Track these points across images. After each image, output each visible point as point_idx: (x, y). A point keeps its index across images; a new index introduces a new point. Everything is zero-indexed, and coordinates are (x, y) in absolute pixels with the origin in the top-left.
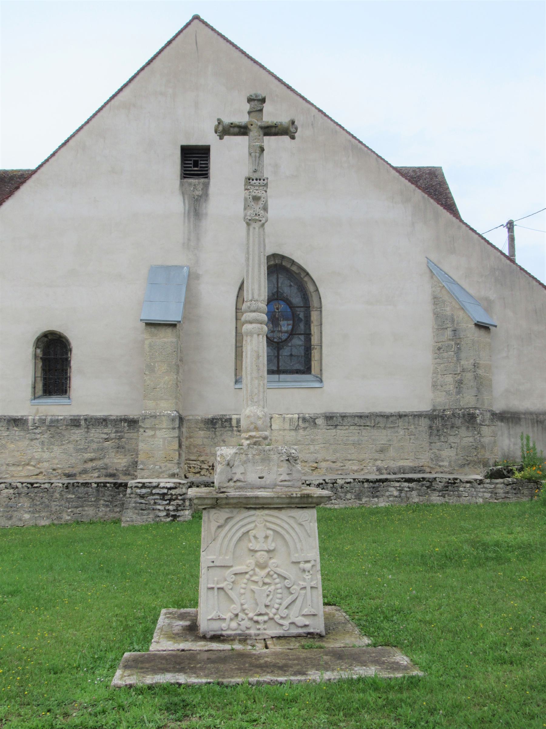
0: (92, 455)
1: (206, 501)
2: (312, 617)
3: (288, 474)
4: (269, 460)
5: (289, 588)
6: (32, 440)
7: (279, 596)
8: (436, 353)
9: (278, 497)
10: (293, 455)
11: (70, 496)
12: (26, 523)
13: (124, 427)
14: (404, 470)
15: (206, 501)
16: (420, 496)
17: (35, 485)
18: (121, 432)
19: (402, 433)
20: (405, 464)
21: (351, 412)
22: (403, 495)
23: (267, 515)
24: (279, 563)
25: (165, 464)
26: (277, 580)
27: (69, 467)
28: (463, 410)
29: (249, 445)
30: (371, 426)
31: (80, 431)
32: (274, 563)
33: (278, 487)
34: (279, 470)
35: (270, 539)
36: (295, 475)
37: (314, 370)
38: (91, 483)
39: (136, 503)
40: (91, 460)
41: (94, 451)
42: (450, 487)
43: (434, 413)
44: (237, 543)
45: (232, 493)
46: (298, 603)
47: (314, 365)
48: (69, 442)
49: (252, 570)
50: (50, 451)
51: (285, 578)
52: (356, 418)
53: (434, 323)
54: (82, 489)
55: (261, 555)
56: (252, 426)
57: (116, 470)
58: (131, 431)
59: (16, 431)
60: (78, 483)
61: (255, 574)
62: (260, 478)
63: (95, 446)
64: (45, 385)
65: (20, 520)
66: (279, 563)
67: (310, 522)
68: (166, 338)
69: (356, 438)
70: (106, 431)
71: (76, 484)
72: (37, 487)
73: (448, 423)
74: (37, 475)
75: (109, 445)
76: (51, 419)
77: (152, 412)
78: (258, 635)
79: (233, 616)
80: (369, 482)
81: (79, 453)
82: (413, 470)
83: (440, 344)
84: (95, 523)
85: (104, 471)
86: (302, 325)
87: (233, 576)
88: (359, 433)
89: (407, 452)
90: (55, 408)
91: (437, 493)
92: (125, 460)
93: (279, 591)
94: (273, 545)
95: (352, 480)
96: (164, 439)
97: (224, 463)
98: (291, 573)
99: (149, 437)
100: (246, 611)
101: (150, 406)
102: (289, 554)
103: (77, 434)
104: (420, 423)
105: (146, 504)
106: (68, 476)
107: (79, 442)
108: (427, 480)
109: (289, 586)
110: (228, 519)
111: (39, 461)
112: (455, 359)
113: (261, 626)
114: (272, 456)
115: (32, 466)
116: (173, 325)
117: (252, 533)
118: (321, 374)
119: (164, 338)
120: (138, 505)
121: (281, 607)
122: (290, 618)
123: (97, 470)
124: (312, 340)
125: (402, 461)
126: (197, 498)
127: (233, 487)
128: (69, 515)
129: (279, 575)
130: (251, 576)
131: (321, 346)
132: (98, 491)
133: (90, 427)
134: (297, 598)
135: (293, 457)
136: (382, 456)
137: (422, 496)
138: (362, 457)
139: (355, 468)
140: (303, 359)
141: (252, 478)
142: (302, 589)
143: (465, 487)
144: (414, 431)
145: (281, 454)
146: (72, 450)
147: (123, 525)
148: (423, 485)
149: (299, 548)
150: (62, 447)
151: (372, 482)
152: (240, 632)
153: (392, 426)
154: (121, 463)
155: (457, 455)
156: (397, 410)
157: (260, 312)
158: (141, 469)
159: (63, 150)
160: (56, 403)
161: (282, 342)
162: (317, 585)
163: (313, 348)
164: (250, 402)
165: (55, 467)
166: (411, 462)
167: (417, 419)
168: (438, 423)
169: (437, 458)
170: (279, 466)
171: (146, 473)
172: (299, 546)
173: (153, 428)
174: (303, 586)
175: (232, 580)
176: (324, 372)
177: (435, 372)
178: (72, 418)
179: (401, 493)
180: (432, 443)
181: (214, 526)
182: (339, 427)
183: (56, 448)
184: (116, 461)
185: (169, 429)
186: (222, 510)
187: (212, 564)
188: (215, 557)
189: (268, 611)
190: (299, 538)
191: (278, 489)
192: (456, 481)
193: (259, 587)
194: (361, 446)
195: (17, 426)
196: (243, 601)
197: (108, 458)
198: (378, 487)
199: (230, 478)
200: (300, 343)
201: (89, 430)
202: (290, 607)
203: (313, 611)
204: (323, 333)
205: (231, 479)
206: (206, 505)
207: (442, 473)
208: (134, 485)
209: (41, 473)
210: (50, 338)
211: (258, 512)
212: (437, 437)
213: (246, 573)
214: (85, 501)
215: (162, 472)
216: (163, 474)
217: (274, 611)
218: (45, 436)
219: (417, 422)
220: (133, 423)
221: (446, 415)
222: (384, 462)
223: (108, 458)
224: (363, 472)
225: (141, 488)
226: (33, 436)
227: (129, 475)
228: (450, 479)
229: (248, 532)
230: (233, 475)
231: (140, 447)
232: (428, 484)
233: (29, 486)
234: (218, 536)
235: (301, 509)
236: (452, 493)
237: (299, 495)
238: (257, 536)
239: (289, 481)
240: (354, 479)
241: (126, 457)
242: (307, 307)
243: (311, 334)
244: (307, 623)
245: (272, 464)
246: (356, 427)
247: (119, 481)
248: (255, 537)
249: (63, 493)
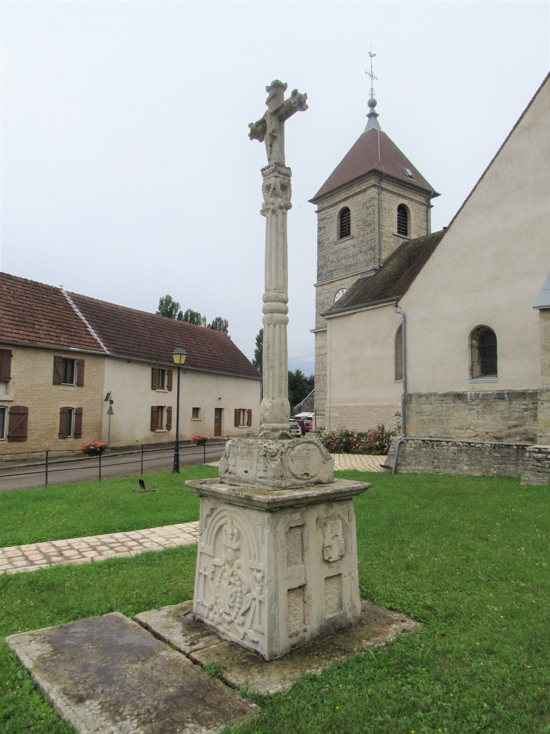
0: (514, 422)
6: (470, 410)
11: (496, 455)
12: (465, 473)
17: (472, 445)
38: (512, 445)
39: (533, 465)
40: (515, 426)
41: (516, 419)
48: (497, 412)
54: (505, 450)
59: (460, 404)
60: (502, 445)
63: (516, 415)
64: (482, 368)
65: (461, 470)
70: (524, 402)
71: (501, 446)
74: (475, 437)
76: (483, 394)
85: (524, 436)
90: (488, 385)
94: (237, 544)
99: (546, 408)
103: (502, 405)
105: (542, 467)
106: (497, 438)
111: (476, 426)
115: (471, 429)
120: (535, 467)
128: (495, 470)
132: (518, 452)
133: (512, 399)
147: (522, 483)
150: (492, 415)
157: (271, 301)
158: (540, 436)
159: (481, 183)
165: (487, 431)
171: (544, 440)
178: (498, 392)
183: (487, 416)
195: (460, 399)
208: (532, 450)
209: (478, 435)
214: (507, 459)
225: (538, 453)
226: (471, 407)
233: (467, 445)
239: (265, 478)
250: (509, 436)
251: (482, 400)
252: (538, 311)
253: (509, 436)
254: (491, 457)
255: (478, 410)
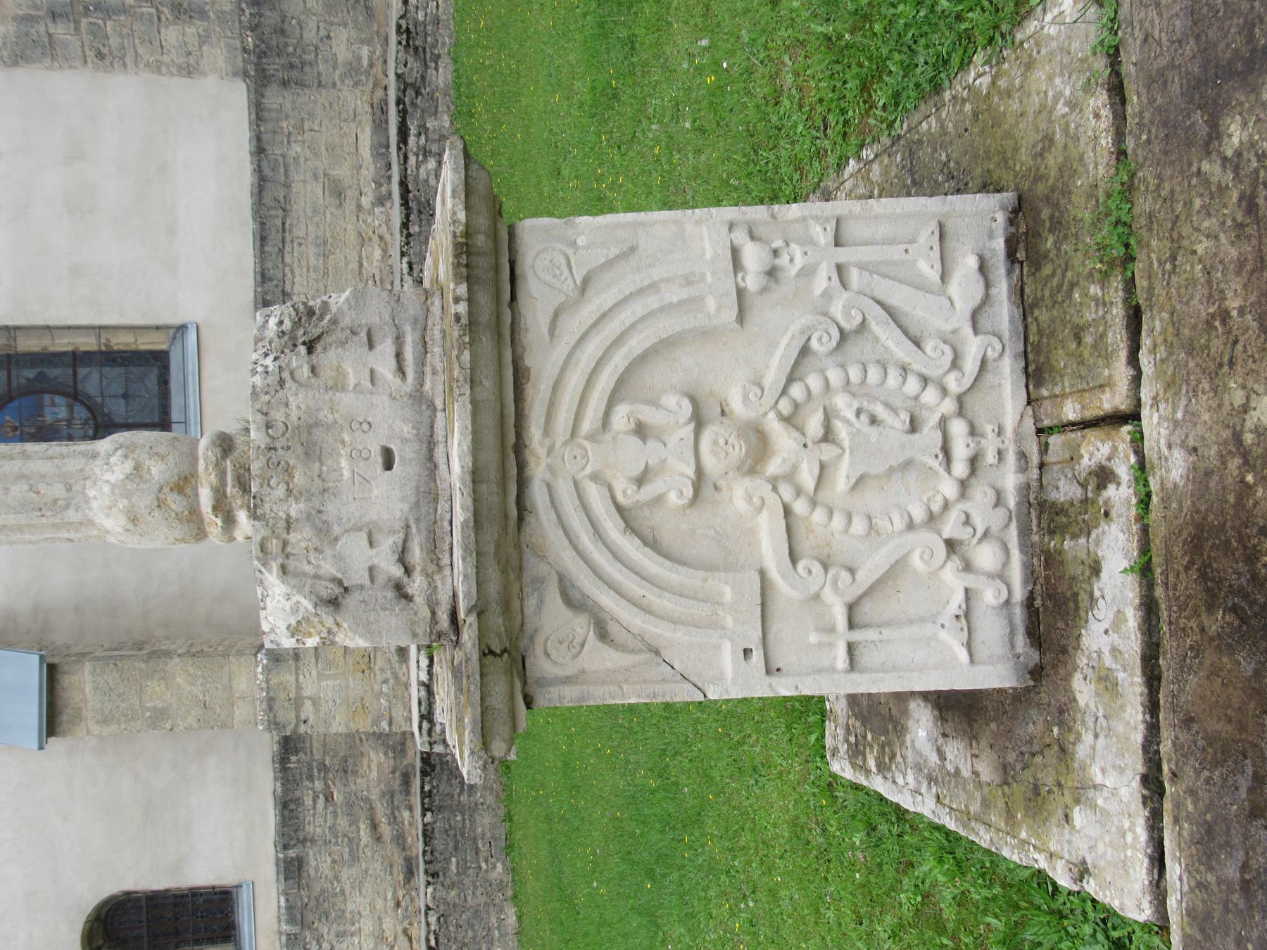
0: (362, 826)
1: (498, 700)
2: (951, 243)
3: (371, 345)
4: (310, 427)
5: (843, 335)
7: (874, 375)
8: (112, 64)
9: (473, 383)
10: (288, 325)
11: (453, 868)
13: (299, 761)
14: (381, 145)
15: (498, 700)
16: (436, 112)
17: (433, 943)
18: (310, 769)
19: (297, 148)
20: (368, 143)
21: (252, 259)
22: (434, 148)
23: (547, 432)
24: (743, 377)
25: (378, 672)
26: (814, 382)
27: (391, 873)
28: (244, 6)
29: (254, 516)
30: (284, 218)
31: (311, 856)
32: (745, 398)
33: (427, 386)
34: (352, 381)
35: (648, 415)
36: (376, 312)
37: (159, 343)
38: (425, 825)
40: (374, 826)
41: (354, 822)
42: (417, 43)
43: (252, 73)
44: (666, 556)
45: (458, 579)
46: (897, 296)
47: (146, 343)
48: (336, 878)
49: (775, 489)
50: (357, 917)
51: (805, 351)
52: (267, 249)
53: (38, 65)
54: (438, 843)
55: (715, 454)
56: (176, 502)
57: (393, 772)
58: (308, 745)
60: (424, 852)
61: (790, 476)
62: (388, 465)
63: (343, 823)
66: (743, 377)
67: (573, 244)
68: (84, 685)
69: (312, 251)
70: (308, 802)
71: (428, 857)
72: (436, 939)
73: (274, 43)
74: (410, 940)
75: (339, 791)
76: (288, 922)
77: (260, 707)
78: (1022, 456)
79: (956, 562)
80: (408, 221)
81: (361, 854)
82: (380, 125)
83: (88, 53)
84: (509, 813)
85: (398, 798)
86: (54, 373)
87: (801, 565)
88: (300, 244)
89: (341, 138)
91: (431, 72)
92: (372, 755)
93: (855, 374)
94: (671, 400)
95: (405, 260)
96: (320, 676)
97: (329, 622)
98: (781, 328)
99: (317, 711)
100: (936, 507)
101: (247, 712)
102: (707, 334)
103: (319, 863)
104: (275, 106)
106: (410, 873)
107: (336, 857)
108: (401, 95)
109: (836, 334)
110: (574, 601)
112: (122, 18)
113: (990, 447)
114: (294, 414)
116: (52, 673)
117: (626, 493)
118: (167, 327)
119: (83, 691)
121: (916, 367)
122: (954, 332)
123: (397, 813)
124: (88, 348)
125: (361, 150)
126: (486, 746)
127: (429, 576)
128: (495, 867)
129: (791, 379)
130: (799, 492)
131: (100, 328)
132: (440, 808)
133: (301, 835)
134: (878, 302)
135: (297, 324)
136: (350, 193)
137: (437, 107)
138: (352, 238)
139: (378, 253)
140: (134, 369)
141: (387, 499)
142: (844, 285)
143: (417, 8)
144: (293, 122)
145: (286, 375)
146: (354, 871)
148: (413, 104)
149: (683, 294)
150: (347, 892)
151: (407, 216)
152: (1013, 531)
153: (282, 170)
154: (380, 764)
155: (345, 25)
156: (248, 158)
158: (390, 724)
160: (249, 916)
161: (95, 418)
162: (827, 220)
163: (106, 346)
164: (71, 515)
165: (391, 904)
166: (362, 131)
167: (266, 114)
168: (274, 65)
169: (353, 70)
170: (338, 385)
171: (398, 713)
172: (673, 295)
173: (298, 703)
174: (835, 277)
175: (817, 568)
176: (160, 322)
177: (157, 68)
178: (282, 877)
179: (430, 151)
180: (320, 82)
181: (598, 658)
182: (288, 288)
183: (350, 906)
184: (375, 774)
185: (297, 669)
186: (529, 628)
187: (757, 656)
188: (727, 647)
189: (934, 419)
190: (640, 292)
191: (434, 387)
192: (404, 27)
193: (840, 457)
194: (330, 240)
196: (899, 524)
197: (368, 791)
198: (419, 203)
199: (390, 594)
200: (95, 376)
201: (309, 837)
202: (913, 331)
203: (928, 236)
204: (70, 322)
205: (399, 588)
206: (512, 697)
207: (385, 62)
208: (426, 738)
209: (405, 931)
210: (101, 942)
211: (538, 471)
212: (307, 69)
213: (787, 511)
214: (462, 835)
215: (396, 677)
216: (400, 675)
217: (930, 395)
218: (326, 931)
219: (273, 115)
220: (289, 746)
221: (256, 46)
222: (364, 190)
223: (368, 791)
224: (387, 237)
227: (403, 744)
228: (400, 43)
229: (620, 509)
230: (381, 579)
231: (342, 730)
232: (410, 92)
234: (640, 637)
235: (520, 283)
236: (429, 39)
237: (463, 289)
238: (637, 470)
239: (399, 340)
240: (403, 254)
241: (365, 752)
242: (9, 363)
243: (74, 353)
244: (972, 262)
245: (326, 416)
246: (288, 249)
247: (418, 764)
248: (640, 481)
249: (448, 882)
250: (400, 840)
251: (303, 924)
252: (51, 740)
253: (400, 840)
254: (461, 882)
255: (333, 934)
